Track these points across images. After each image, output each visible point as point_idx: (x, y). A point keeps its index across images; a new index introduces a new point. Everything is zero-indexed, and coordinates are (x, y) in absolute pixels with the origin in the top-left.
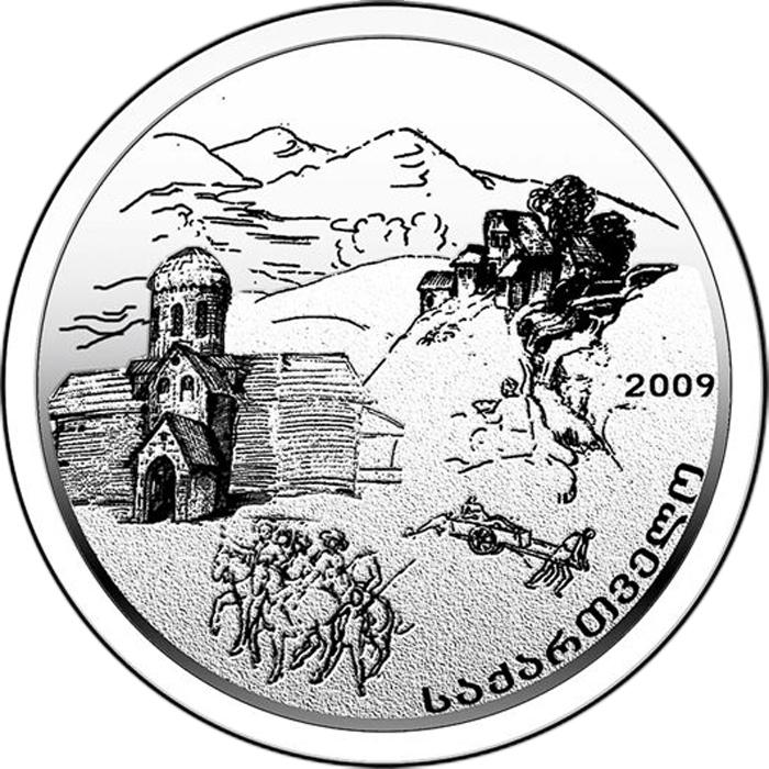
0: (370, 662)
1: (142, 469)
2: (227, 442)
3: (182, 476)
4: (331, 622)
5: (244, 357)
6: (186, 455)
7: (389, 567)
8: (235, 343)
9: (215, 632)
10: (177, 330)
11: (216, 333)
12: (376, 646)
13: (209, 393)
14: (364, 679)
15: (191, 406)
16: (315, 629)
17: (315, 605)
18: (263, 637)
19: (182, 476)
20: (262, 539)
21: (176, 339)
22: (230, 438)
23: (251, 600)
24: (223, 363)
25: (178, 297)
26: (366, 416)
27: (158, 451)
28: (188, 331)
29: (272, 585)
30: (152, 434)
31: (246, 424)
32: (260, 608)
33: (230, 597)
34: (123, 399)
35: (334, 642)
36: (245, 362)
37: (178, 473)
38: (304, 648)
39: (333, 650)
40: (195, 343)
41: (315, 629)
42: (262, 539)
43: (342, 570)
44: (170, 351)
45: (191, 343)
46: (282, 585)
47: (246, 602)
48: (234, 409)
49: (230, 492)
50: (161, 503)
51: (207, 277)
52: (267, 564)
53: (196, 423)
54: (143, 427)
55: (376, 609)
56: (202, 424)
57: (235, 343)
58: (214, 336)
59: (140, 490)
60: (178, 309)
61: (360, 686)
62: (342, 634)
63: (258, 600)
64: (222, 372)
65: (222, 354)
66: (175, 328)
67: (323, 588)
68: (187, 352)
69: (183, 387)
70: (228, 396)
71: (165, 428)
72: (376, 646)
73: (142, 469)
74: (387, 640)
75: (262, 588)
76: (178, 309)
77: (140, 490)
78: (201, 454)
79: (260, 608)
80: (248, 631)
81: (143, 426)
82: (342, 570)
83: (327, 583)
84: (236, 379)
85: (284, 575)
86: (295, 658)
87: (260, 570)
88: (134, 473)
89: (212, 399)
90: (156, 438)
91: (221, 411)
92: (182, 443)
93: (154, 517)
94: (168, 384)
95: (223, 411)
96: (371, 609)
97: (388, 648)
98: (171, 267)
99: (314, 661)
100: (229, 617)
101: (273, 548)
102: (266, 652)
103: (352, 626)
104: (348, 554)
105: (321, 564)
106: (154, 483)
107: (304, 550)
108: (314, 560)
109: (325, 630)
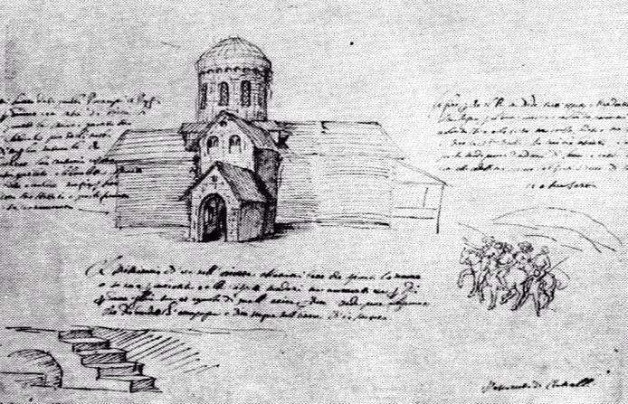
0: (542, 303)
1: (196, 202)
2: (273, 185)
3: (233, 209)
4: (523, 283)
5: (286, 124)
6: (236, 193)
7: (554, 259)
8: (276, 113)
9: (461, 287)
10: (224, 99)
11: (260, 104)
12: (547, 295)
13: (255, 147)
14: (539, 309)
15: (242, 158)
16: (515, 287)
17: (516, 277)
18: (486, 291)
19: (233, 209)
20: (487, 246)
21: (224, 108)
22: (275, 181)
23: (480, 274)
24: (265, 126)
25: (223, 77)
26: (400, 169)
27: (210, 190)
28: (234, 105)
29: (492, 267)
30: (203, 177)
31: (289, 170)
32: (485, 277)
33: (470, 272)
34: (179, 149)
35: (524, 293)
36: (286, 128)
37: (229, 207)
38: (508, 295)
39: (524, 296)
40: (240, 111)
41: (515, 287)
42: (487, 246)
43: (529, 261)
44: (217, 117)
45: (237, 111)
46: (497, 266)
47: (477, 275)
48: (278, 159)
49: (276, 221)
50: (215, 227)
51: (251, 62)
52: (489, 257)
53: (245, 170)
54: (196, 171)
55: (548, 279)
56: (250, 171)
57: (276, 113)
58: (258, 107)
59: (195, 218)
60: (224, 86)
61: (538, 313)
62: (528, 289)
63: (484, 274)
64: (267, 133)
65: (265, 120)
66: (221, 100)
67: (520, 269)
68: (232, 117)
69: (231, 142)
70: (272, 150)
71: (215, 172)
72: (547, 295)
73: (196, 202)
74: (553, 293)
75: (486, 268)
76: (224, 86)
77: (195, 218)
78: (250, 191)
79: (485, 277)
80: (478, 288)
81: (196, 170)
82: (529, 261)
83: (521, 266)
84: (279, 138)
85: (498, 262)
86: (503, 299)
87: (485, 260)
88: (189, 204)
89: (257, 152)
90: (208, 180)
91: (266, 161)
92: (232, 185)
93: (208, 238)
94: (217, 140)
95: (269, 159)
96: (544, 278)
97: (552, 296)
98: (216, 54)
99: (511, 303)
100: (469, 281)
101: (493, 250)
102: (488, 298)
103: (534, 288)
104: (533, 254)
105: (518, 258)
106: (207, 213)
107: (510, 251)
108: (515, 256)
109: (520, 288)
